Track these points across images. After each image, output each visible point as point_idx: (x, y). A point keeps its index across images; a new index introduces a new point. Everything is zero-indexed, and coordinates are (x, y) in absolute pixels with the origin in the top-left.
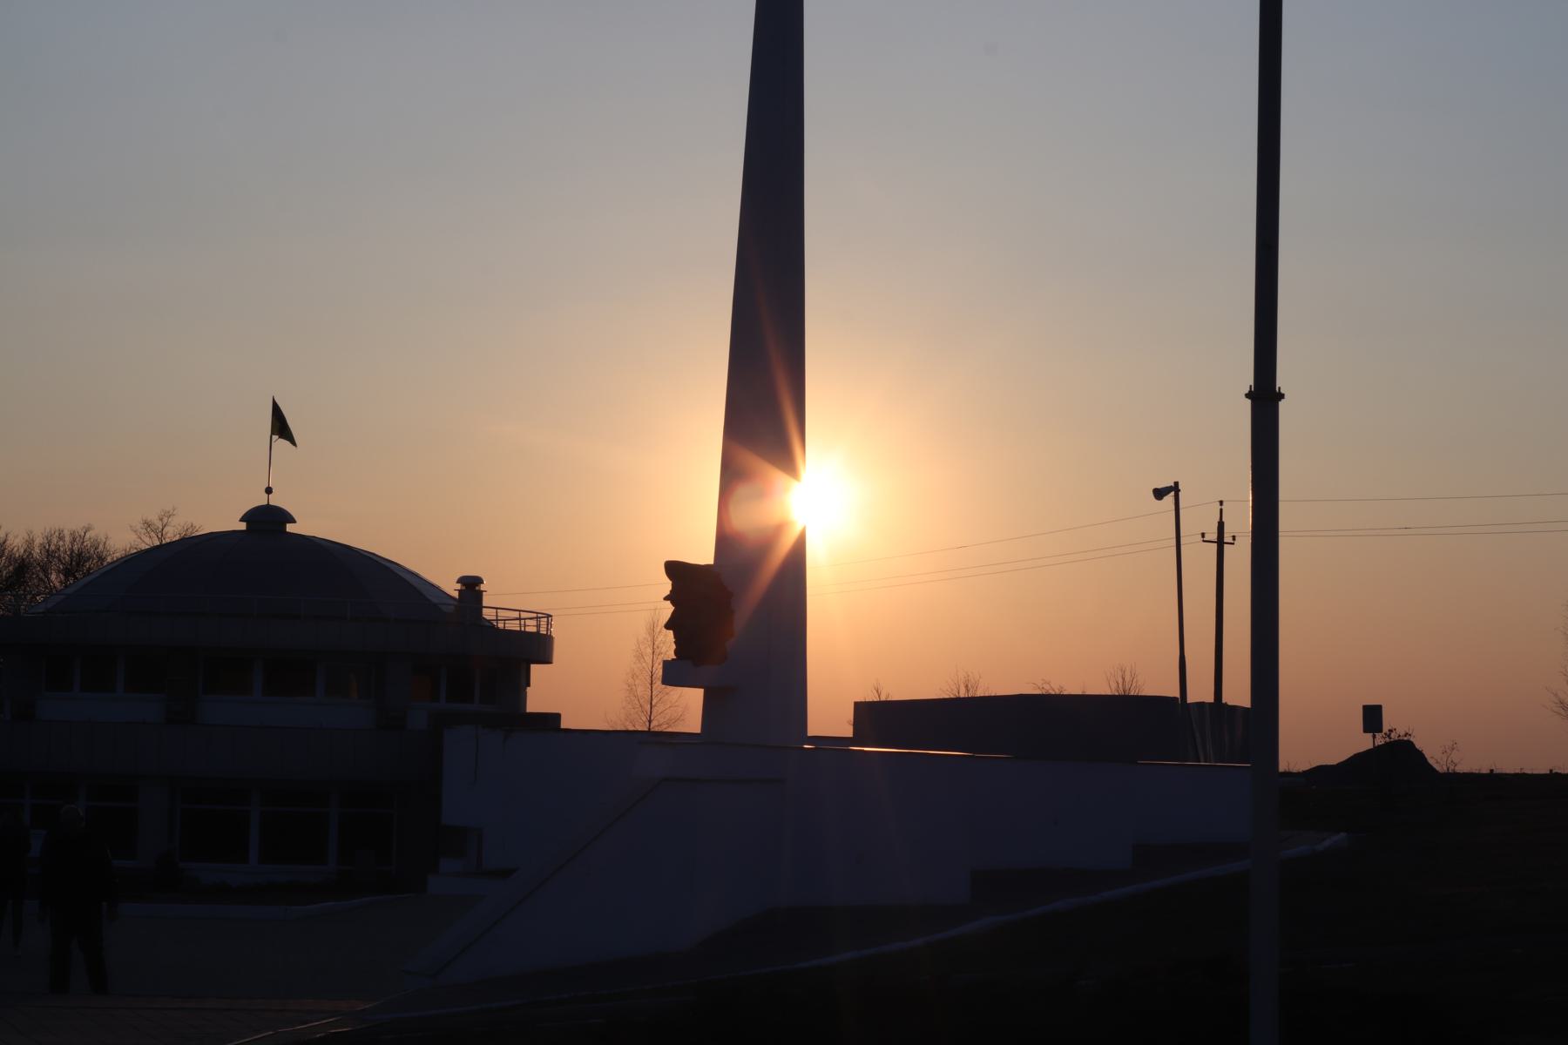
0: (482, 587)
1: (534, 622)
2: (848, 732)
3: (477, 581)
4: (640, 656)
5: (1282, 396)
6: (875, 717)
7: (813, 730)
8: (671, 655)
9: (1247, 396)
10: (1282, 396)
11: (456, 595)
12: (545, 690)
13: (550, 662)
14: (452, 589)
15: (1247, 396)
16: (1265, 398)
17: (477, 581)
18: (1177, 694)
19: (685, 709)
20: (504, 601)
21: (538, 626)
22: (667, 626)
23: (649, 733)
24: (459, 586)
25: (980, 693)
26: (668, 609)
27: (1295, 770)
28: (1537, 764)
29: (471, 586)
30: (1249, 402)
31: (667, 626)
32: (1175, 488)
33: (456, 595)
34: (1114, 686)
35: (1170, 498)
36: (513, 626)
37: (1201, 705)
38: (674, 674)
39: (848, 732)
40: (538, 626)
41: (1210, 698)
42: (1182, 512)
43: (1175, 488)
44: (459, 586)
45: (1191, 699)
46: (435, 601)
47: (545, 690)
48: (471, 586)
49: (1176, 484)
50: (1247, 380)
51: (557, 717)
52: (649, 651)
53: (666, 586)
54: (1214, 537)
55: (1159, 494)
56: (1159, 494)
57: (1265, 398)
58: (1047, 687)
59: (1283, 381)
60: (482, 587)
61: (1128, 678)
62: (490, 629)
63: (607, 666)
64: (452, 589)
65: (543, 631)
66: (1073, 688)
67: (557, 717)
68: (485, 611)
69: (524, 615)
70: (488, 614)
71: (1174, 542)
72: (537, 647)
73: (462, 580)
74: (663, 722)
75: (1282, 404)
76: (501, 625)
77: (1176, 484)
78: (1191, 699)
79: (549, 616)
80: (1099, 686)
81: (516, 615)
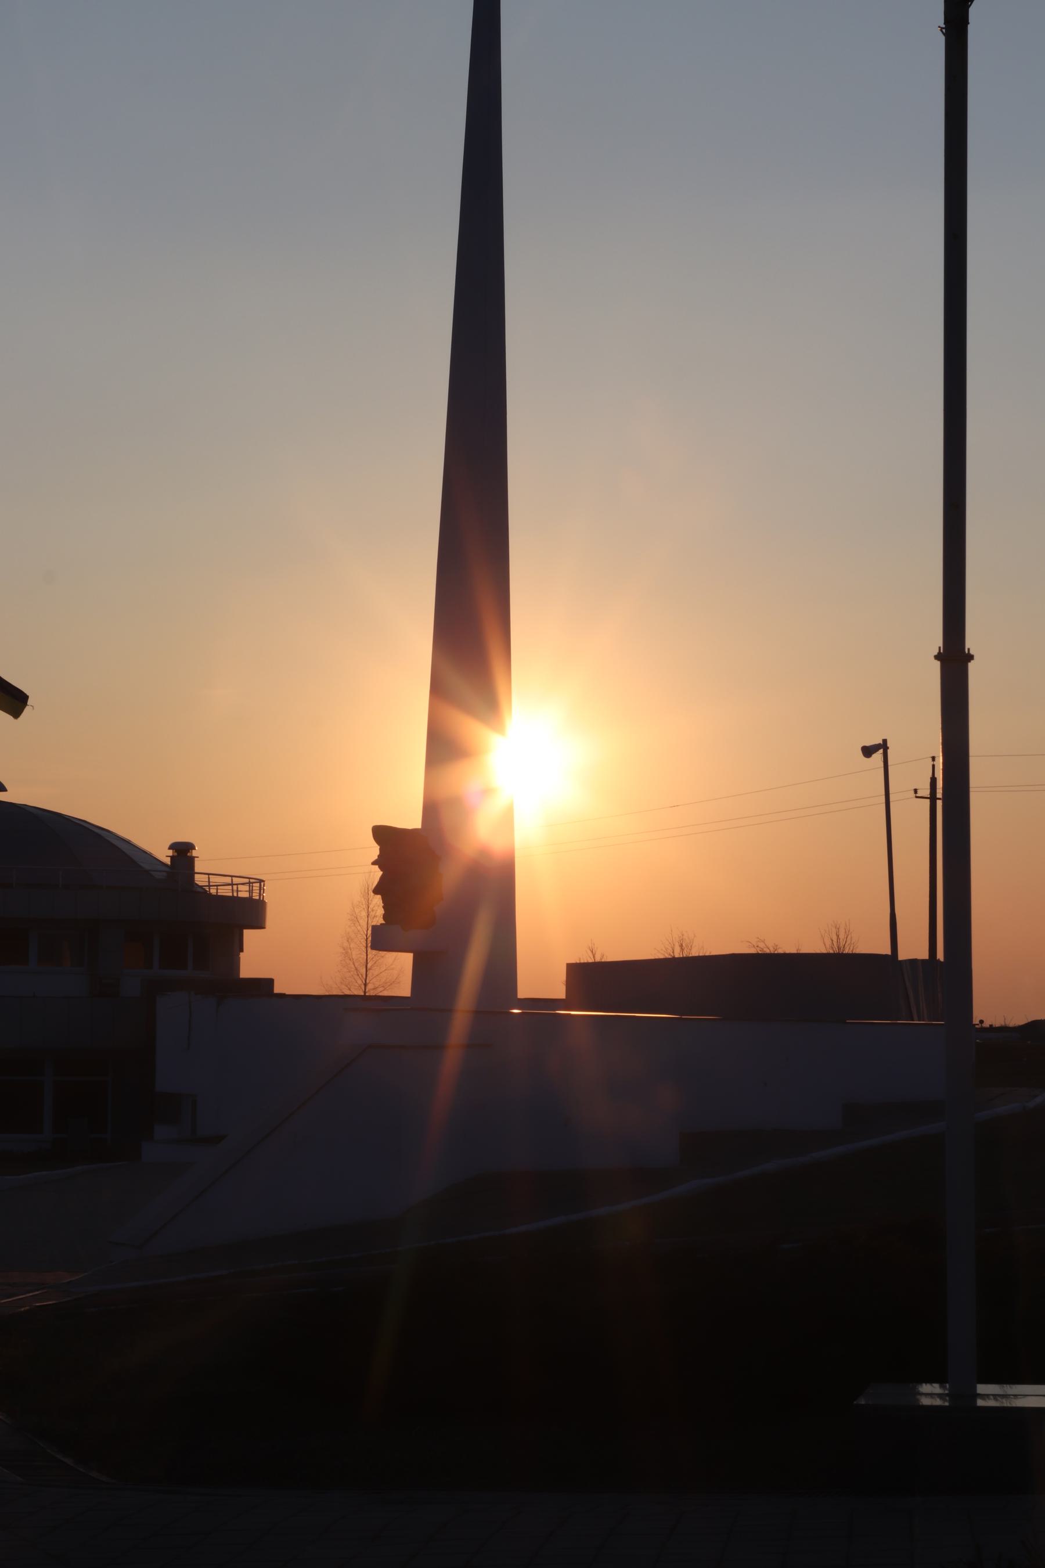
0: (194, 853)
1: (246, 888)
2: (559, 992)
3: (190, 847)
4: (355, 920)
5: (971, 657)
6: (592, 979)
7: (524, 991)
8: (379, 920)
9: (937, 657)
10: (971, 657)
11: (168, 861)
12: (257, 956)
13: (264, 928)
14: (164, 855)
15: (937, 657)
16: (954, 660)
17: (190, 847)
18: (889, 952)
19: (396, 973)
20: (212, 867)
21: (251, 891)
22: (376, 891)
23: (365, 998)
24: (170, 853)
25: (695, 953)
26: (377, 873)
27: (1012, 1025)
28: (652, 957)
29: (183, 851)
30: (938, 664)
31: (376, 891)
32: (884, 746)
33: (168, 861)
34: (828, 943)
35: (878, 756)
36: (225, 892)
37: (913, 962)
38: (381, 939)
39: (559, 992)
40: (251, 891)
41: (924, 955)
42: (890, 768)
43: (884, 746)
44: (170, 853)
45: (903, 955)
46: (147, 867)
47: (257, 956)
48: (183, 851)
49: (885, 741)
50: (936, 641)
51: (270, 982)
52: (364, 914)
53: (374, 851)
54: (927, 792)
55: (868, 751)
56: (868, 751)
57: (954, 660)
58: (762, 945)
59: (971, 643)
60: (194, 853)
61: (842, 936)
62: (202, 895)
63: (316, 935)
64: (164, 855)
65: (256, 896)
66: (788, 948)
67: (270, 982)
68: (197, 876)
69: (236, 880)
70: (200, 880)
71: (892, 798)
72: (249, 912)
73: (173, 847)
74: (378, 987)
75: (971, 665)
76: (213, 891)
77: (885, 741)
78: (903, 955)
79: (261, 881)
80: (813, 944)
81: (228, 880)
